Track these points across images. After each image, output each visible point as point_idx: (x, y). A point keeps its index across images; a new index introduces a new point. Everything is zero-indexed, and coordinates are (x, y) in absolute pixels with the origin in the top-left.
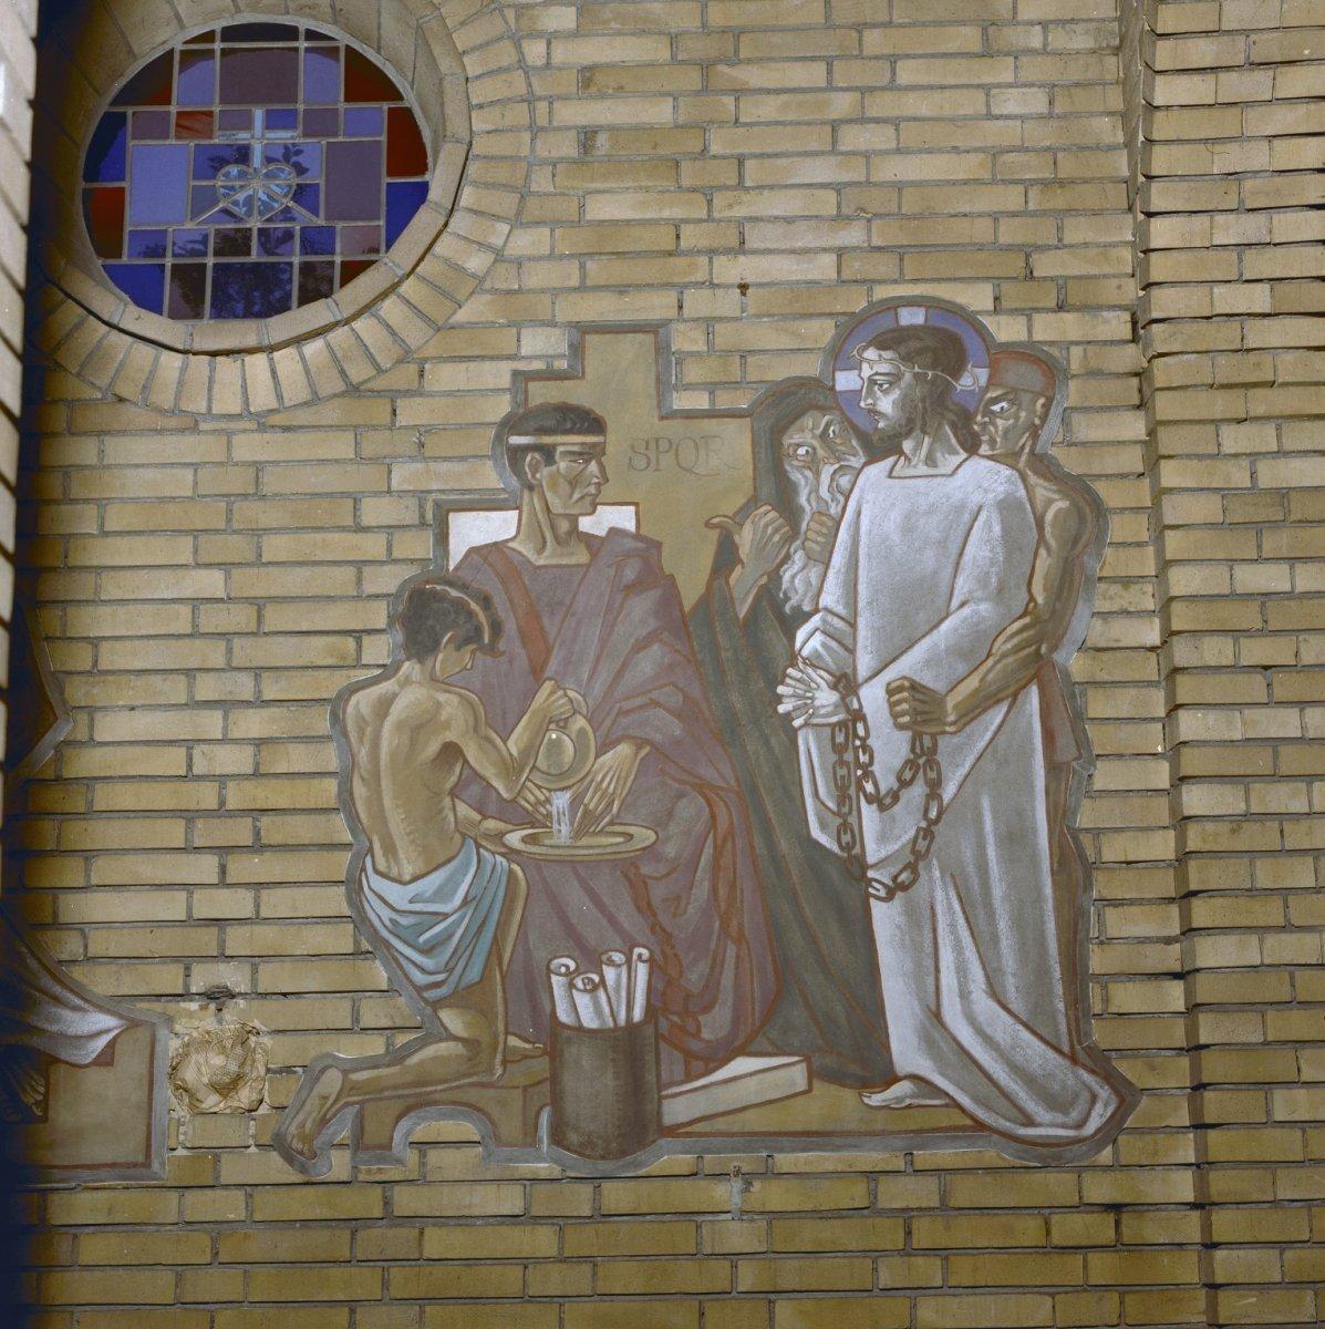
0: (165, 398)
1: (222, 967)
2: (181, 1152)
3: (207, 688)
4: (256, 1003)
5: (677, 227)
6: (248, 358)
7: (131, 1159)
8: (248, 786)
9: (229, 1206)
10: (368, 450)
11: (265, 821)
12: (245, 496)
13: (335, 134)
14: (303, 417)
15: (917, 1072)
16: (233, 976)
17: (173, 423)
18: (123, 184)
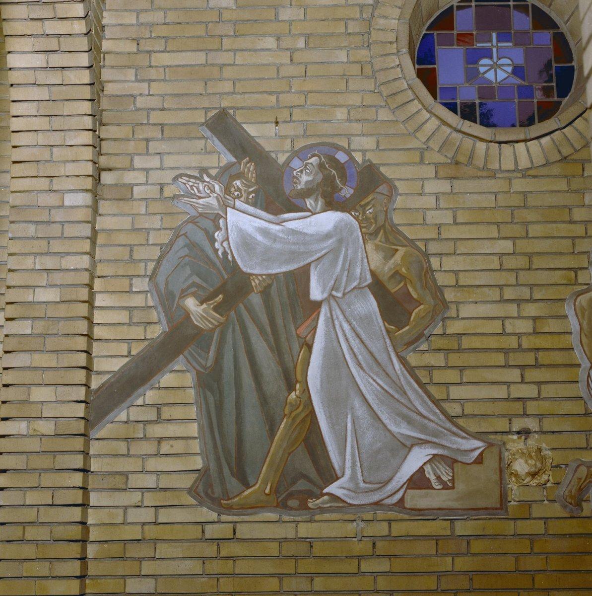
0: (479, 162)
1: (526, 419)
2: (513, 503)
3: (509, 294)
4: (543, 436)
6: (516, 145)
7: (494, 506)
8: (532, 338)
9: (538, 527)
10: (574, 186)
11: (541, 353)
12: (519, 207)
14: (543, 171)
15: (331, 492)
16: (532, 424)
17: (484, 174)
18: (435, 66)
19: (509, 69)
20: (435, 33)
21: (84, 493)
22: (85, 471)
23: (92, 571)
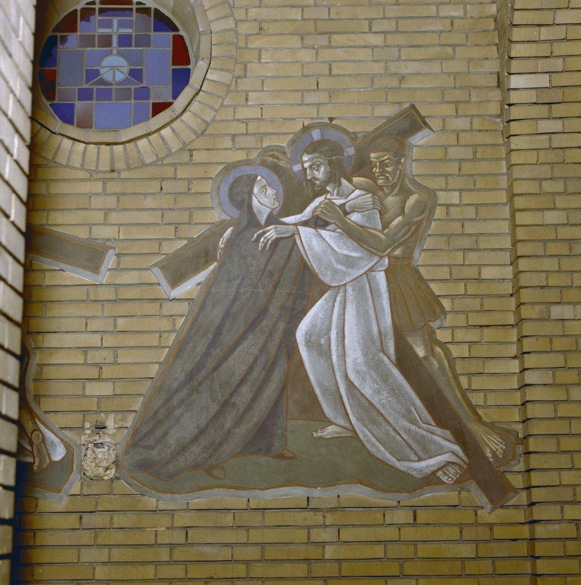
5: (330, 65)
13: (81, 85)
19: (126, 70)
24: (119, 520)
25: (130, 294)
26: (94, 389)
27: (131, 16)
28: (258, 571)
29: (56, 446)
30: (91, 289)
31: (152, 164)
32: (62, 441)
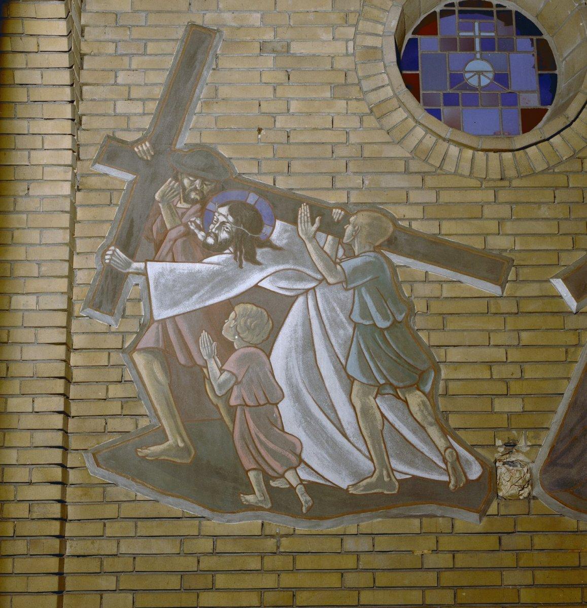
19: (491, 75)
20: (421, 92)
21: (61, 542)
22: (63, 484)
23: (69, 586)
24: (539, 541)
25: (532, 306)
26: (501, 405)
27: (493, 19)
28: (367, 598)
29: (471, 464)
30: (492, 301)
31: (543, 172)
32: (477, 459)
